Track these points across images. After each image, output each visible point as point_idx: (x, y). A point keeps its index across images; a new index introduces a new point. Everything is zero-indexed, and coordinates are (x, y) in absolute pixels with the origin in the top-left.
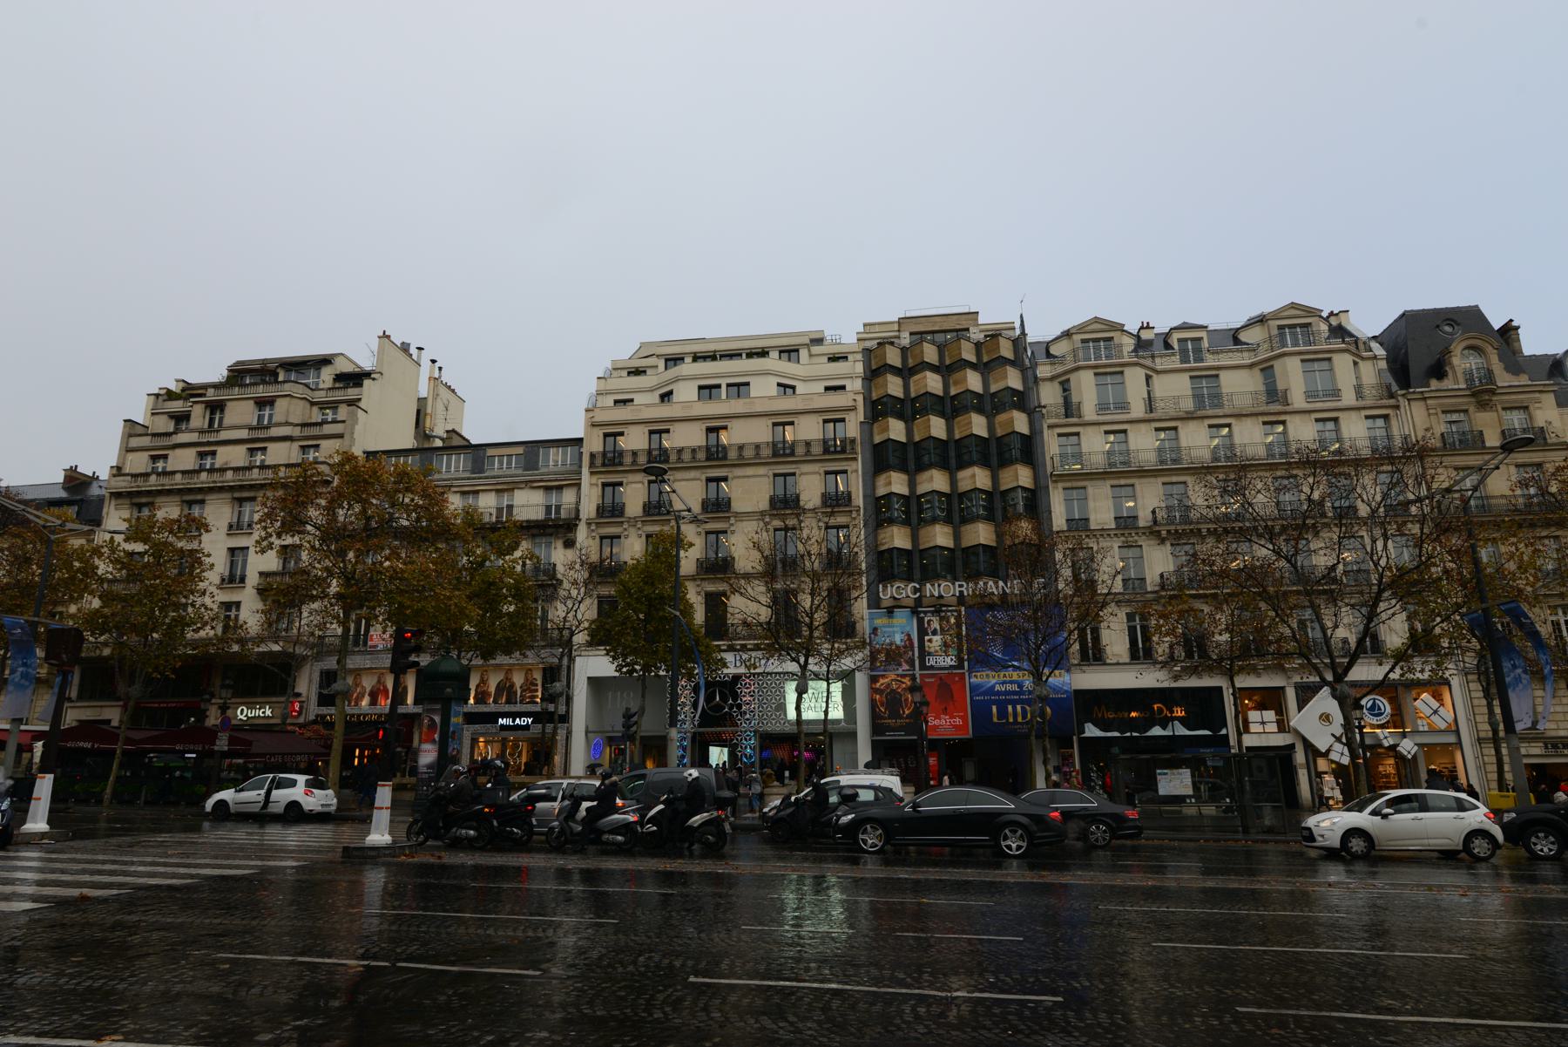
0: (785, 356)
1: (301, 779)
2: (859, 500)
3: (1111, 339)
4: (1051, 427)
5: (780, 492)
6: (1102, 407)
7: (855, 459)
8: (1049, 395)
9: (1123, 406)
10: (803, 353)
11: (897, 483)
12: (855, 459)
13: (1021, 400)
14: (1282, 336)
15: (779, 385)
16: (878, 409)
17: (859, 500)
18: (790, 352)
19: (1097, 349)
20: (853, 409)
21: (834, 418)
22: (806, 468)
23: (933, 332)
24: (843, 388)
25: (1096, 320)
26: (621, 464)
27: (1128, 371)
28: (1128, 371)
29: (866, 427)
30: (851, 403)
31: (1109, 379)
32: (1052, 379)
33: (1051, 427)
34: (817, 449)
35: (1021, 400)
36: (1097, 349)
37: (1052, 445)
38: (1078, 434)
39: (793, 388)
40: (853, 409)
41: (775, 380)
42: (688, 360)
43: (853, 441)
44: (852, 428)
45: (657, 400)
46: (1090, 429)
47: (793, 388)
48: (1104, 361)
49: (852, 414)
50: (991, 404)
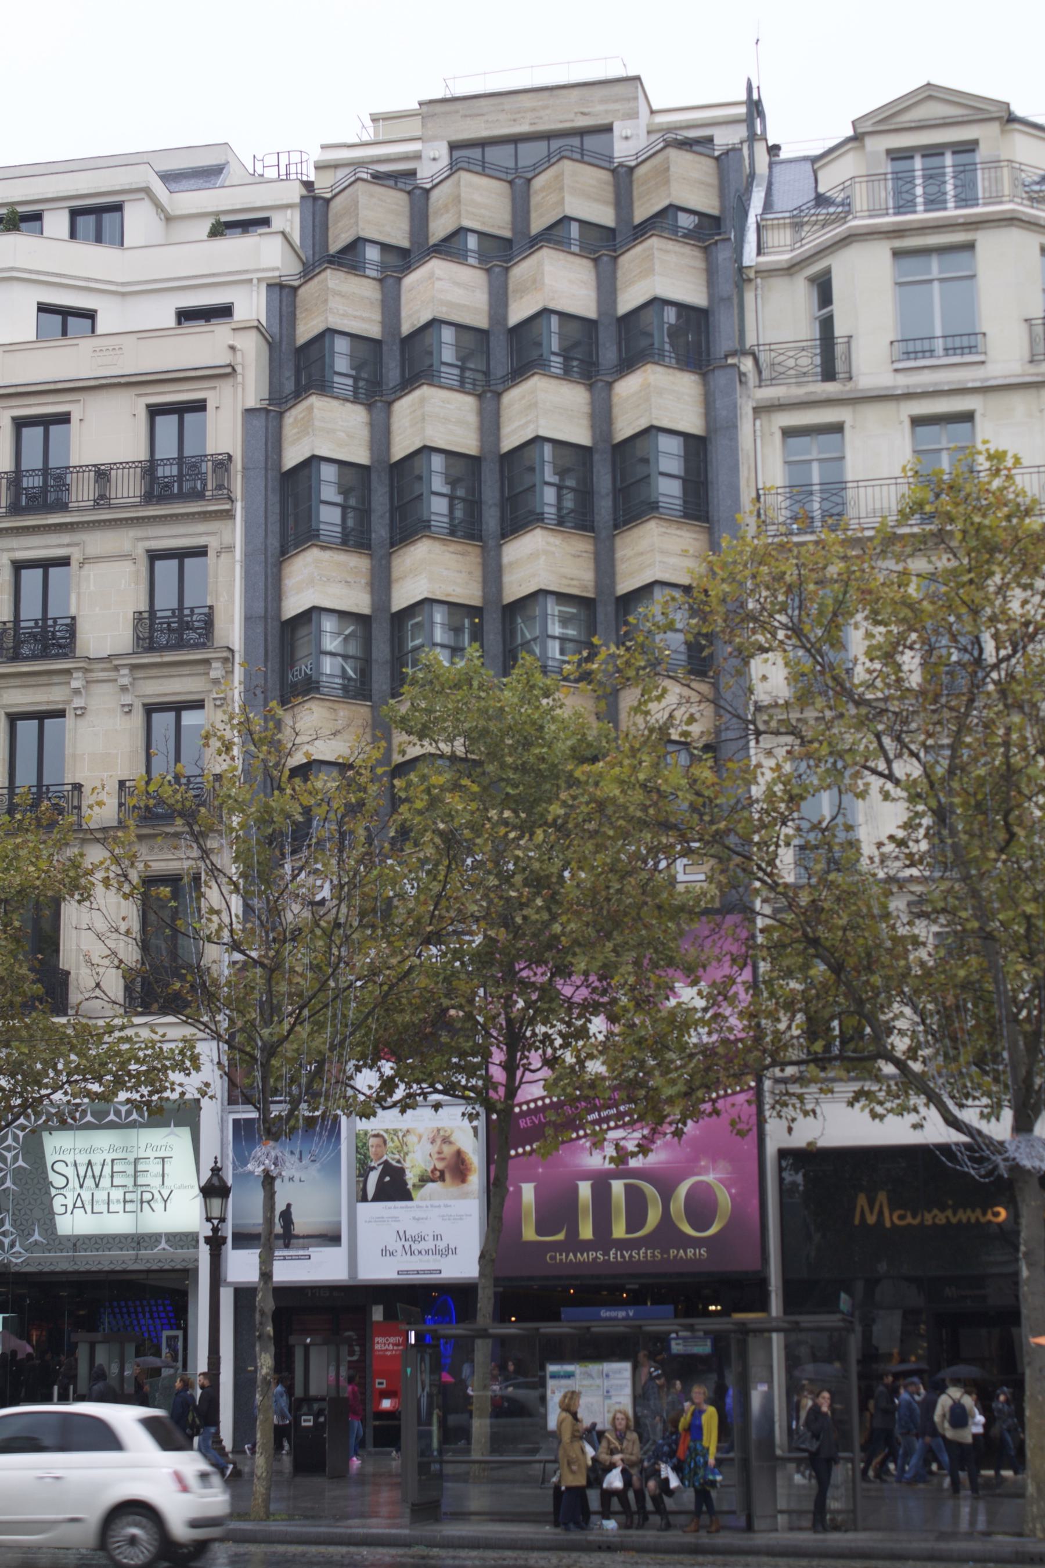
0: (87, 223)
1: (124, 1418)
2: (232, 629)
3: (969, 147)
4: (761, 410)
5: (167, 601)
6: (911, 348)
7: (228, 515)
8: (778, 318)
9: (967, 343)
10: (137, 219)
11: (323, 581)
12: (228, 515)
13: (695, 339)
14: (902, 182)
15: (43, 309)
16: (300, 367)
17: (232, 629)
18: (96, 218)
19: (933, 177)
20: (228, 373)
21: (176, 409)
22: (97, 542)
23: (515, 140)
24: (225, 311)
25: (930, 93)
26: (62, 507)
27: (987, 242)
28: (987, 242)
29: (259, 422)
30: (223, 358)
31: (935, 266)
32: (790, 269)
33: (761, 410)
34: (127, 488)
35: (695, 339)
36: (933, 177)
37: (762, 465)
38: (838, 428)
39: (90, 315)
40: (228, 373)
41: (29, 298)
42: (57, 223)
43: (223, 464)
44: (223, 432)
45: (171, 321)
46: (872, 414)
47: (90, 315)
48: (921, 215)
49: (225, 388)
50: (601, 348)
